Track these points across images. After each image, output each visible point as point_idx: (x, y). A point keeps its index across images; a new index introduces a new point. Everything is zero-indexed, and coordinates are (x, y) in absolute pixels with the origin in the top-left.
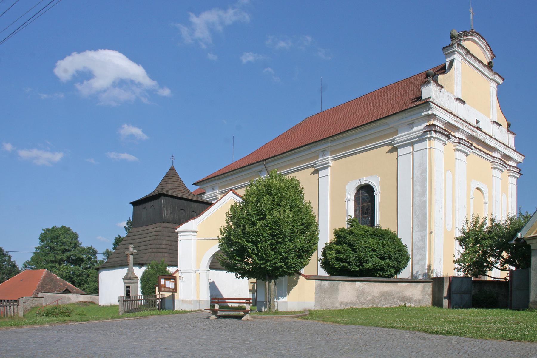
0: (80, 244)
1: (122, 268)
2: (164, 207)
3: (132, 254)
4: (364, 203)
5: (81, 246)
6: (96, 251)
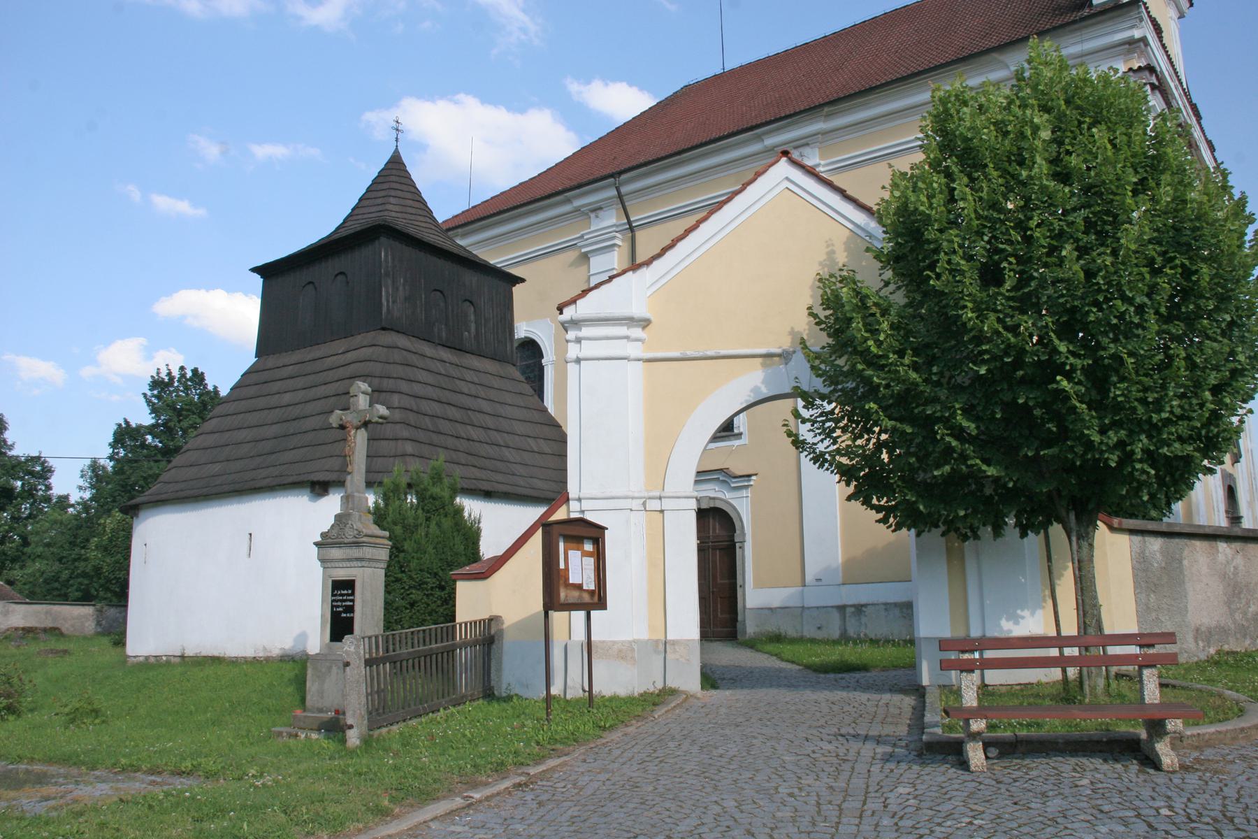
0: (10, 450)
1: (239, 503)
2: (387, 274)
3: (366, 424)
5: (10, 453)
6: (51, 467)
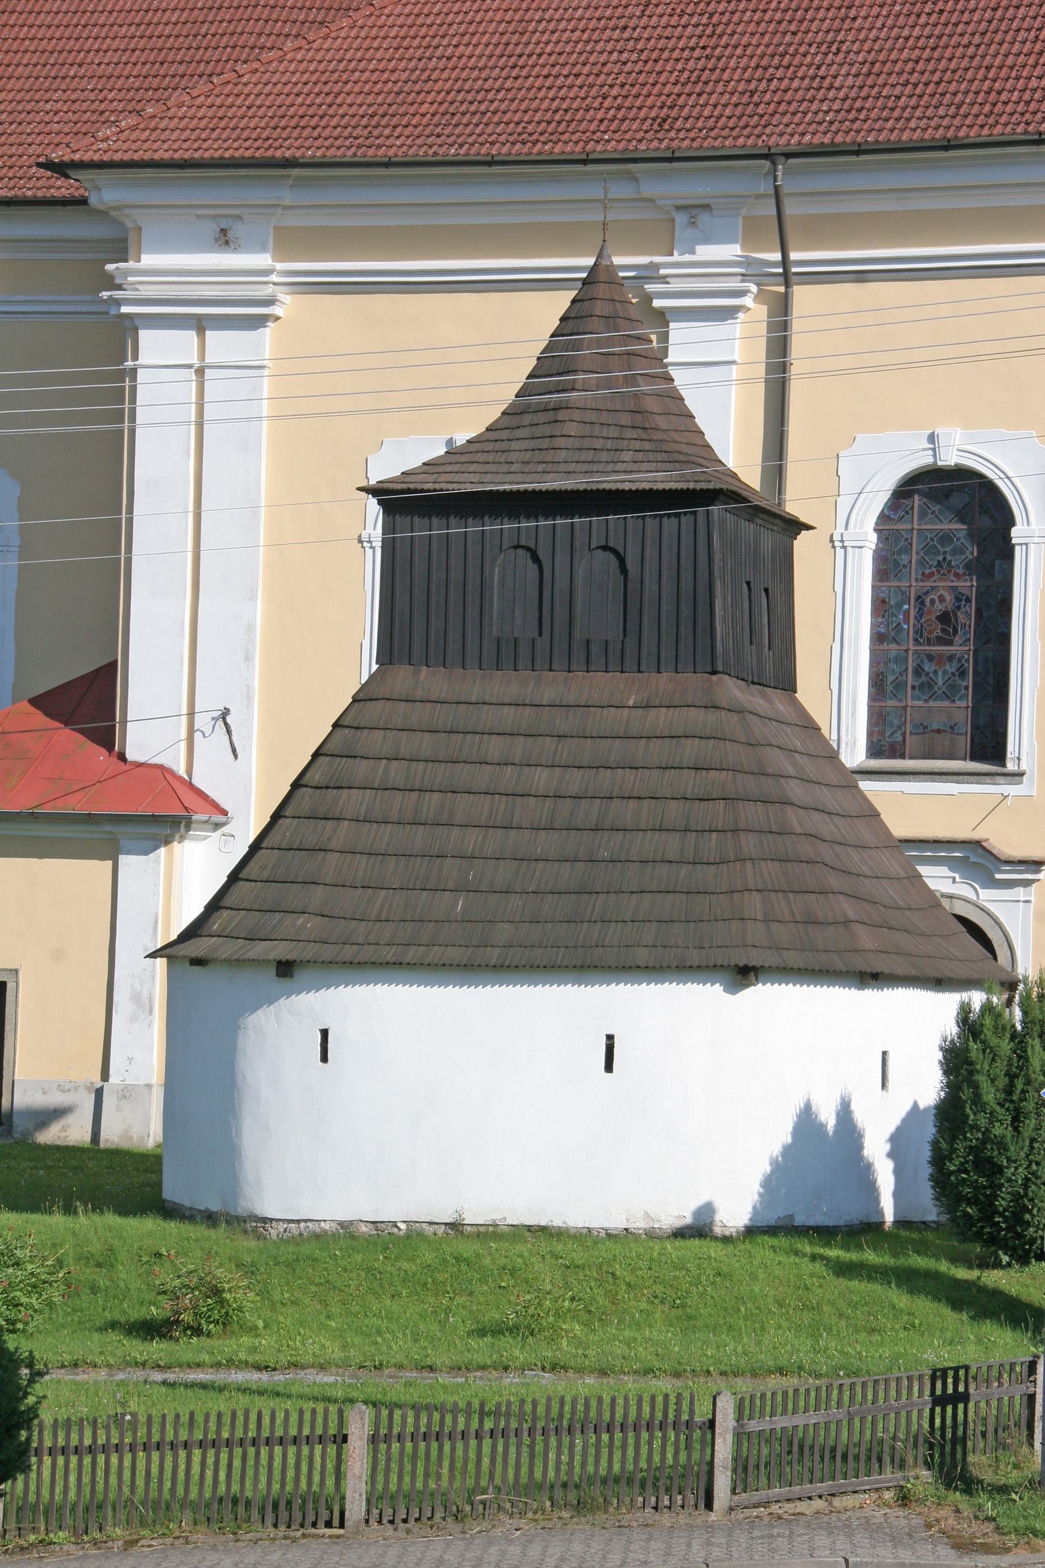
4: (932, 574)
